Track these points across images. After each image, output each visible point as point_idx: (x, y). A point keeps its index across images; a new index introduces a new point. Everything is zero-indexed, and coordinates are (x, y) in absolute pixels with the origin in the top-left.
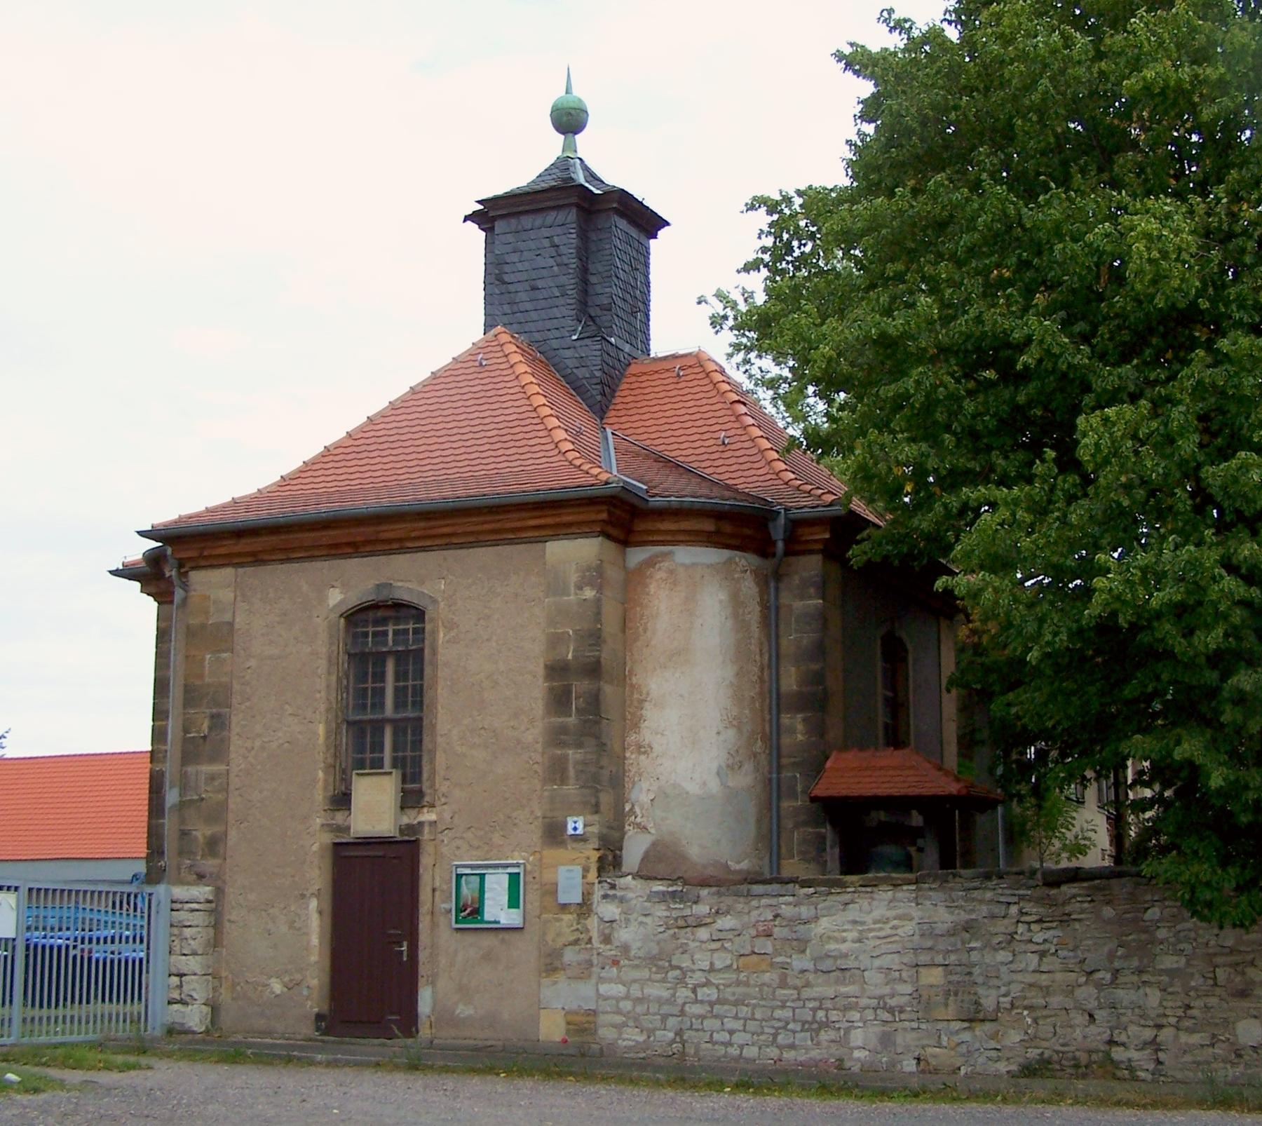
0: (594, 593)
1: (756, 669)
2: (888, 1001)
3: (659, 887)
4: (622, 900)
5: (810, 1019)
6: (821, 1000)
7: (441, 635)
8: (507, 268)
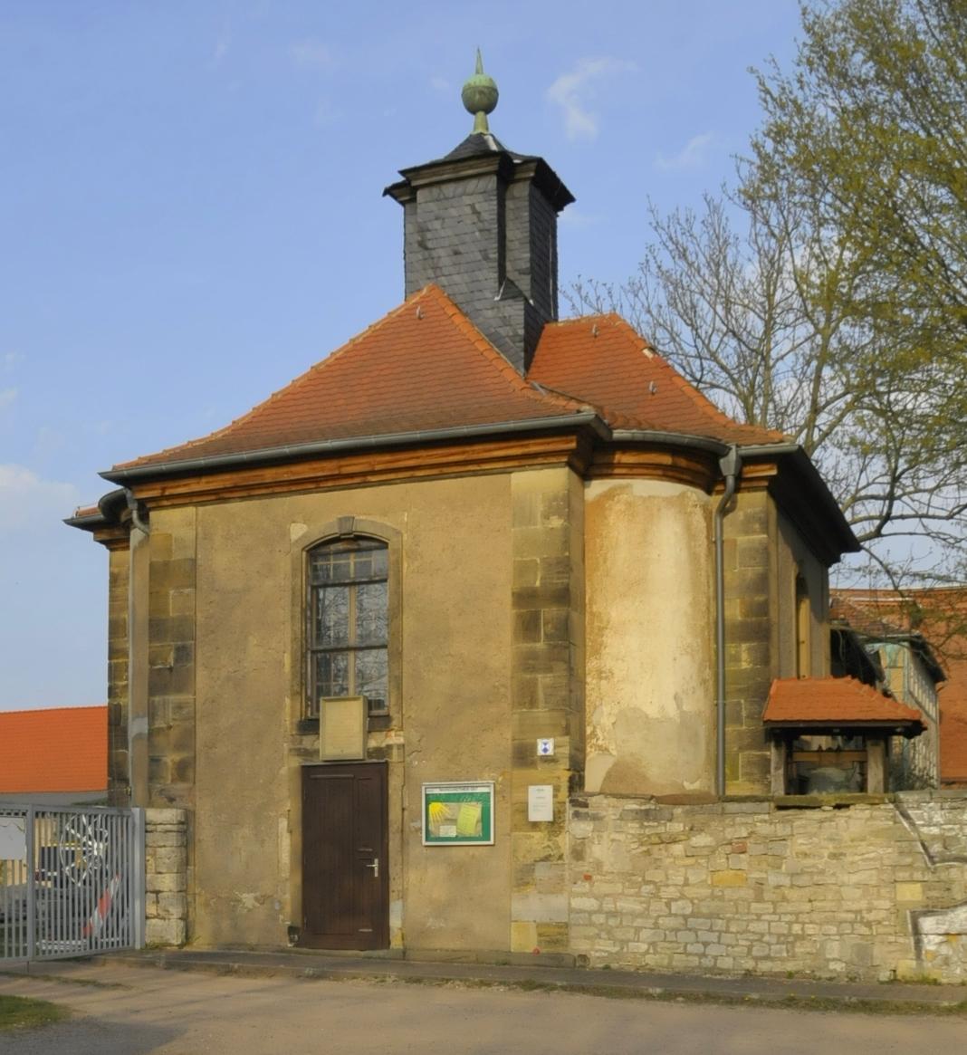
0: (561, 522)
1: (705, 600)
2: (865, 915)
3: (632, 805)
4: (595, 818)
5: (786, 932)
6: (797, 914)
7: (405, 565)
8: (429, 235)
